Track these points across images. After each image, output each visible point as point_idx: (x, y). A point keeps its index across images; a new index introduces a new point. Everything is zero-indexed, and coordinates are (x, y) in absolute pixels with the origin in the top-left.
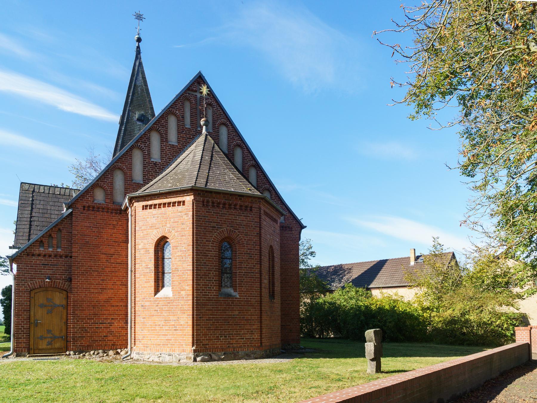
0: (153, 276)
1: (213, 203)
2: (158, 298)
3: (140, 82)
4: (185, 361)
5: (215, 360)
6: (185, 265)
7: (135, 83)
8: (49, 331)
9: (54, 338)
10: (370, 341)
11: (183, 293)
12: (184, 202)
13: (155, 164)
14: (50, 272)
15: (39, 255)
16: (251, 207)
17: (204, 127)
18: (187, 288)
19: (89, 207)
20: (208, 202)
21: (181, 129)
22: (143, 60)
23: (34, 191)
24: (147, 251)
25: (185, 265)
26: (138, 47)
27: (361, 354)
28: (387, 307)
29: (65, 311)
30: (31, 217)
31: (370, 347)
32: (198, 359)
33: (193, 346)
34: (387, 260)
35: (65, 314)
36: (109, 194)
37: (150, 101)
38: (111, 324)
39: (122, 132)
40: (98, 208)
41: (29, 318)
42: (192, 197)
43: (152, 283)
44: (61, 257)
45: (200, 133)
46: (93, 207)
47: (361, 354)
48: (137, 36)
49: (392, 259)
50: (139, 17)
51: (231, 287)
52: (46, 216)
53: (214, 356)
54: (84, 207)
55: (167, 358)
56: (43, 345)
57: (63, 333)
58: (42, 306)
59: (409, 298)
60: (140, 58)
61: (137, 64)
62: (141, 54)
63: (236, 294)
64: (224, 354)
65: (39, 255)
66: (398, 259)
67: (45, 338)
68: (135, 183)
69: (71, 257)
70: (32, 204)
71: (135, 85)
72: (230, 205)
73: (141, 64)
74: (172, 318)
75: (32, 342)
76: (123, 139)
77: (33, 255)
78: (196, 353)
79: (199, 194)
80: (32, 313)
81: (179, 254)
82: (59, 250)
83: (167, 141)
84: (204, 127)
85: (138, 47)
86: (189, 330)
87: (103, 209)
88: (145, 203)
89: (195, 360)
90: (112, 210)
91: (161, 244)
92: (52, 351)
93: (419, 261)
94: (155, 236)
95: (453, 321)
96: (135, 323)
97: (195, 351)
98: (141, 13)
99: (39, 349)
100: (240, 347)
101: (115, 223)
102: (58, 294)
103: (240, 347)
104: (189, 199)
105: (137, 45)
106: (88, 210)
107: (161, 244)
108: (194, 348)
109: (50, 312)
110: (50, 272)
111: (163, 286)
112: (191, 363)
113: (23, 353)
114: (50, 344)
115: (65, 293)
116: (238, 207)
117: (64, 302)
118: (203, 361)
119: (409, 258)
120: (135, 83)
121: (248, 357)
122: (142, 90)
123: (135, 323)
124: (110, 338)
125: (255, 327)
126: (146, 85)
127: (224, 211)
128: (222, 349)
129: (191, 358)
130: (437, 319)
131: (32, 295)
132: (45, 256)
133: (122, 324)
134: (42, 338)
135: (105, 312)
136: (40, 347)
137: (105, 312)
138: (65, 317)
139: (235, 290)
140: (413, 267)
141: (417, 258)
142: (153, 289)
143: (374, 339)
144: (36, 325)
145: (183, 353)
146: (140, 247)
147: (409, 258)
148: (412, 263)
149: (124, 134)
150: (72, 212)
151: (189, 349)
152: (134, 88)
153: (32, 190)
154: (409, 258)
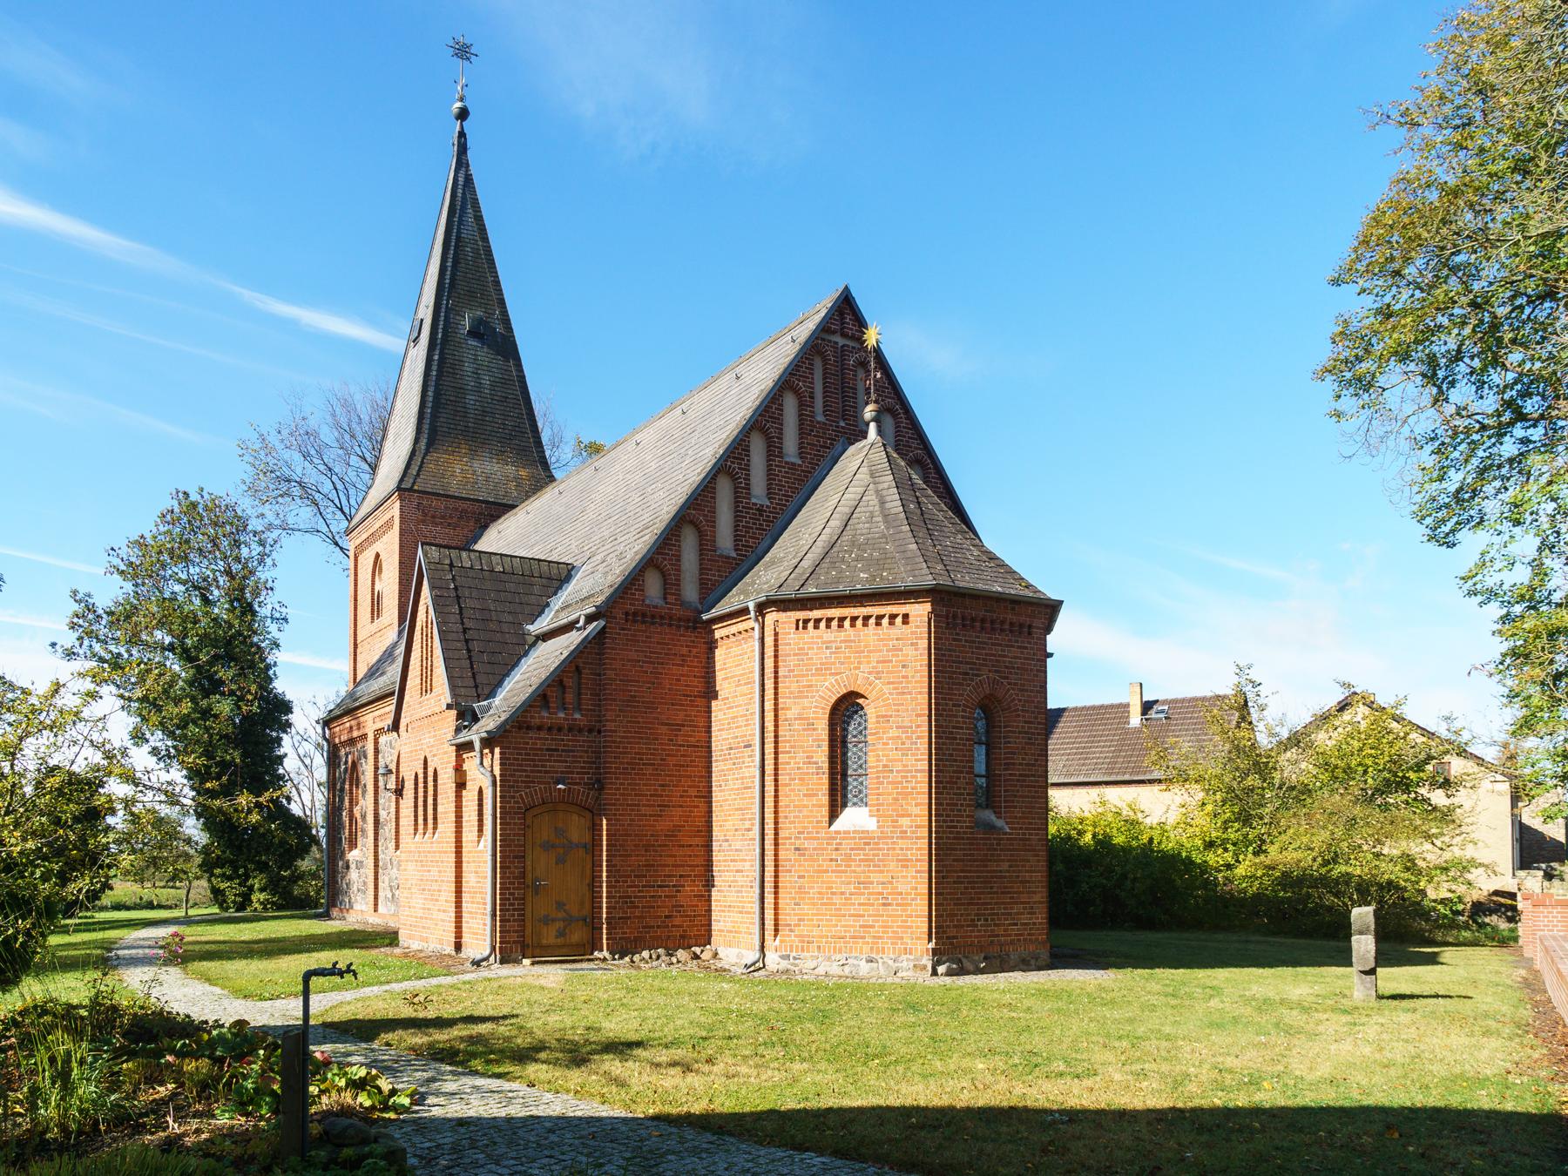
0: (827, 782)
1: (963, 619)
2: (837, 832)
3: (469, 231)
4: (910, 973)
5: (968, 973)
6: (910, 760)
7: (459, 232)
8: (560, 905)
9: (569, 920)
10: (1361, 933)
11: (905, 821)
12: (906, 616)
13: (760, 510)
14: (560, 767)
15: (539, 728)
16: (1030, 627)
17: (873, 426)
18: (916, 810)
19: (635, 614)
20: (955, 617)
21: (806, 426)
22: (473, 170)
23: (451, 565)
24: (811, 726)
25: (910, 760)
26: (462, 134)
27: (1344, 958)
28: (1119, 840)
29: (589, 858)
30: (465, 631)
31: (1364, 945)
32: (941, 969)
33: (930, 940)
34: (1064, 710)
35: (589, 866)
36: (671, 585)
37: (497, 283)
38: (678, 887)
39: (435, 368)
40: (653, 617)
41: (523, 875)
42: (928, 607)
43: (824, 799)
44: (580, 730)
45: (864, 435)
46: (644, 615)
47: (1344, 958)
48: (459, 104)
49: (1075, 709)
50: (463, 52)
51: (987, 807)
52: (492, 626)
53: (968, 965)
54: (627, 614)
55: (864, 968)
56: (549, 936)
57: (586, 911)
58: (547, 846)
59: (1165, 812)
60: (468, 165)
61: (461, 180)
62: (469, 153)
63: (1000, 823)
64: (985, 958)
65: (539, 728)
66: (1093, 708)
67: (554, 920)
68: (721, 556)
69: (599, 732)
70: (458, 597)
71: (458, 238)
72: (992, 622)
73: (469, 180)
74: (874, 877)
75: (528, 932)
76: (437, 385)
77: (529, 728)
78: (938, 955)
79: (942, 599)
80: (529, 863)
81: (893, 733)
82: (577, 716)
83: (781, 455)
84: (873, 426)
85: (462, 134)
86: (921, 905)
87: (662, 617)
88: (802, 615)
89: (935, 973)
90: (680, 620)
91: (846, 709)
92: (564, 951)
93: (1152, 714)
94: (831, 690)
95: (1290, 880)
96: (776, 887)
97: (935, 952)
98: (468, 42)
99: (542, 947)
100: (1012, 943)
101: (685, 650)
102: (575, 817)
103: (1012, 943)
104: (920, 611)
105: (458, 128)
106: (635, 621)
107: (846, 709)
108: (932, 945)
109: (560, 861)
110: (560, 767)
111: (844, 805)
112: (925, 978)
113: (513, 956)
114: (561, 934)
115: (589, 815)
116: (1007, 626)
117: (587, 838)
118: (949, 973)
119: (1127, 705)
120: (459, 232)
121: (1025, 965)
122: (476, 251)
123: (776, 887)
124: (677, 921)
125: (1037, 898)
126: (485, 239)
127: (984, 637)
128: (981, 948)
129: (925, 967)
130: (1245, 871)
131: (529, 822)
132: (550, 729)
133: (699, 888)
134: (547, 920)
135: (670, 861)
136: (544, 942)
137: (670, 861)
138: (588, 872)
139: (998, 814)
140: (1138, 731)
141: (1147, 707)
142: (825, 811)
143: (1373, 927)
144: (536, 890)
145: (904, 957)
146: (790, 714)
147: (1124, 708)
148: (1135, 720)
149: (440, 371)
150: (603, 631)
151: (922, 949)
152: (456, 246)
153: (447, 561)
154: (1127, 705)
